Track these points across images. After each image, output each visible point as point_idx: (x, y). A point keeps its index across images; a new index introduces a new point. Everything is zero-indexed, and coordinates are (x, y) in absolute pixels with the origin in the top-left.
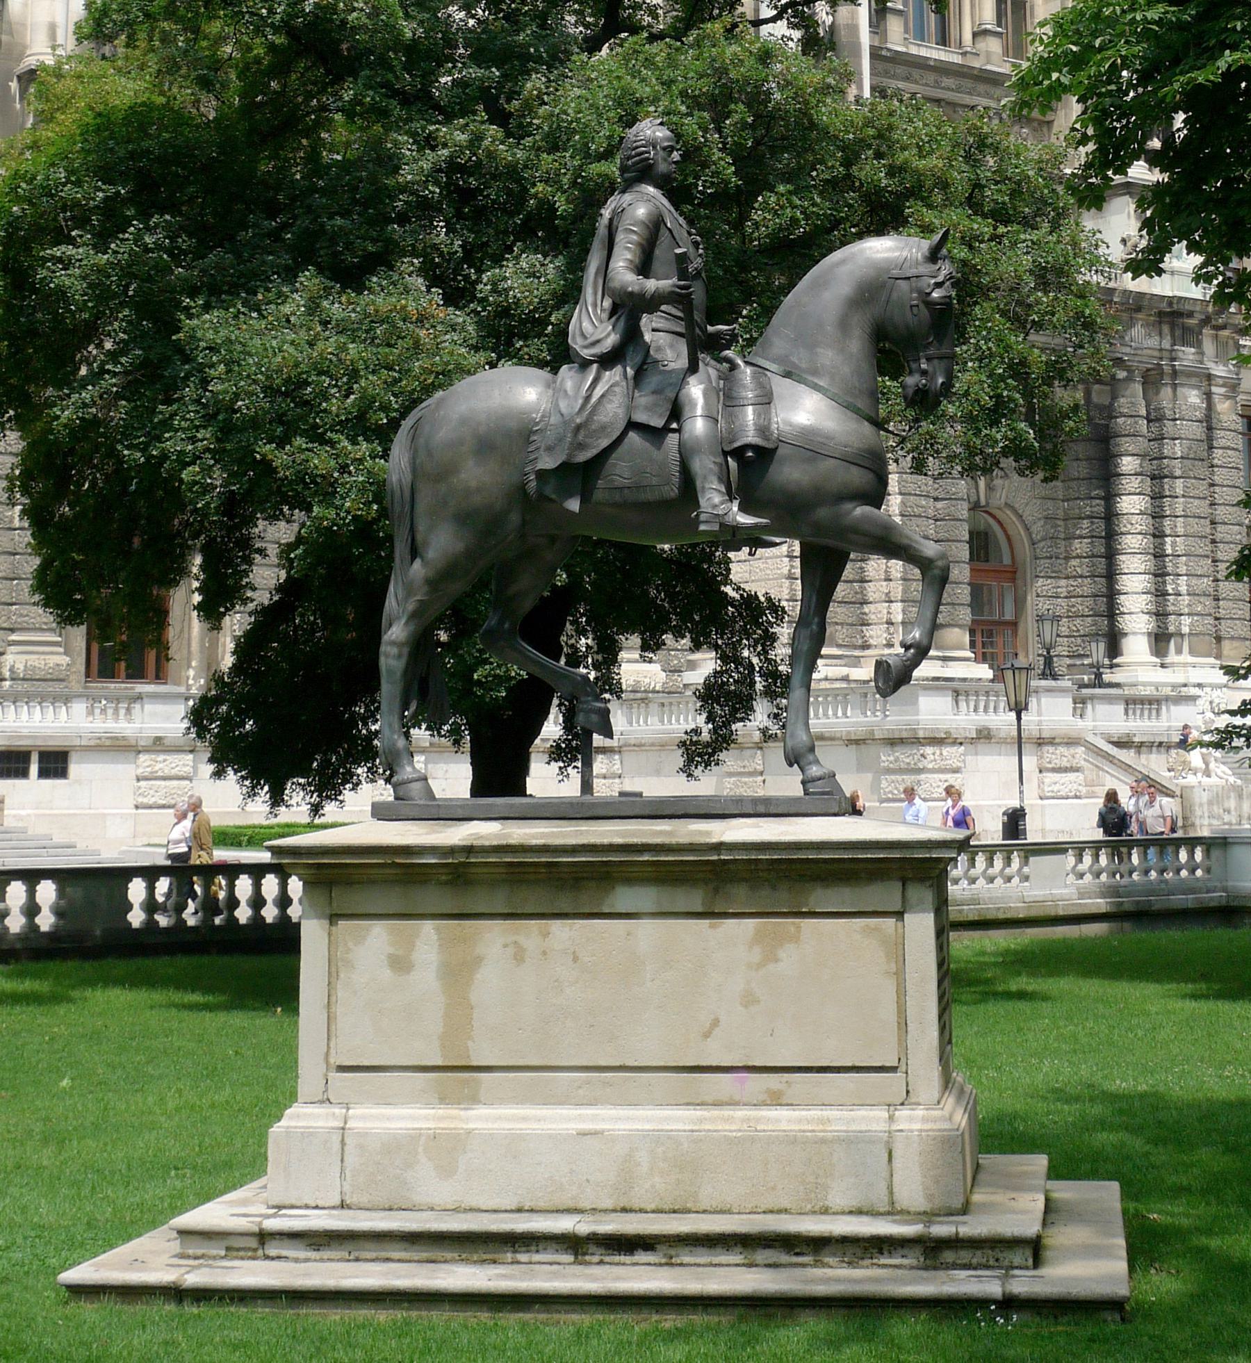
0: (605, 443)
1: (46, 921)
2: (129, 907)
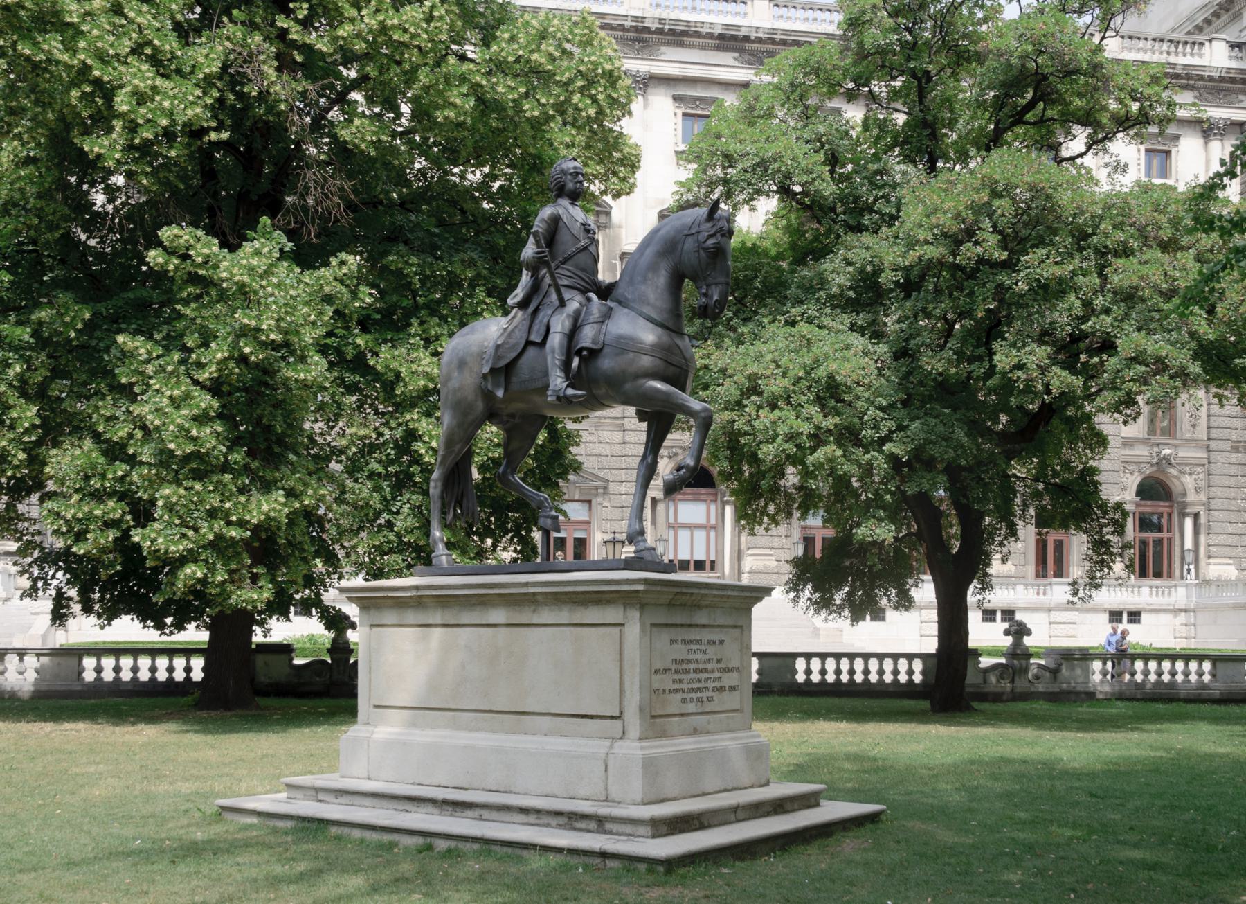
0: (514, 355)
1: (918, 678)
2: (797, 672)
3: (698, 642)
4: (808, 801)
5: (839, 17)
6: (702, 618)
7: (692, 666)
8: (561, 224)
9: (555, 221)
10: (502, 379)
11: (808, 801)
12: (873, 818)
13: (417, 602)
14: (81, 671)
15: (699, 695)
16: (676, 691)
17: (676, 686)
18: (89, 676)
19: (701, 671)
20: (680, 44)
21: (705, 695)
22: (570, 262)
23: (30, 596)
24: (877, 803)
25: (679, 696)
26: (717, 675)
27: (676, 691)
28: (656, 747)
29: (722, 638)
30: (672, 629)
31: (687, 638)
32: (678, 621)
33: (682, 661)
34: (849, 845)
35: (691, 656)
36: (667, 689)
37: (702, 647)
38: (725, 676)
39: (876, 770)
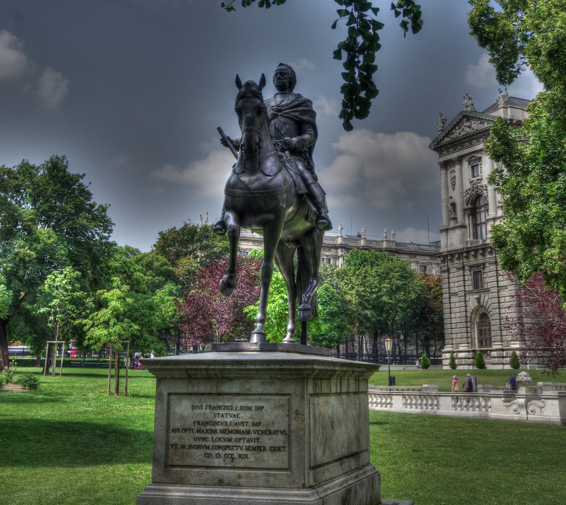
3: (231, 408)
5: (514, 291)
6: (226, 388)
7: (219, 428)
15: (228, 452)
16: (199, 447)
17: (198, 443)
19: (231, 432)
21: (236, 453)
26: (253, 436)
27: (199, 447)
28: (282, 495)
29: (260, 404)
30: (193, 398)
31: (213, 404)
32: (196, 390)
33: (207, 423)
36: (187, 444)
39: (260, 163)
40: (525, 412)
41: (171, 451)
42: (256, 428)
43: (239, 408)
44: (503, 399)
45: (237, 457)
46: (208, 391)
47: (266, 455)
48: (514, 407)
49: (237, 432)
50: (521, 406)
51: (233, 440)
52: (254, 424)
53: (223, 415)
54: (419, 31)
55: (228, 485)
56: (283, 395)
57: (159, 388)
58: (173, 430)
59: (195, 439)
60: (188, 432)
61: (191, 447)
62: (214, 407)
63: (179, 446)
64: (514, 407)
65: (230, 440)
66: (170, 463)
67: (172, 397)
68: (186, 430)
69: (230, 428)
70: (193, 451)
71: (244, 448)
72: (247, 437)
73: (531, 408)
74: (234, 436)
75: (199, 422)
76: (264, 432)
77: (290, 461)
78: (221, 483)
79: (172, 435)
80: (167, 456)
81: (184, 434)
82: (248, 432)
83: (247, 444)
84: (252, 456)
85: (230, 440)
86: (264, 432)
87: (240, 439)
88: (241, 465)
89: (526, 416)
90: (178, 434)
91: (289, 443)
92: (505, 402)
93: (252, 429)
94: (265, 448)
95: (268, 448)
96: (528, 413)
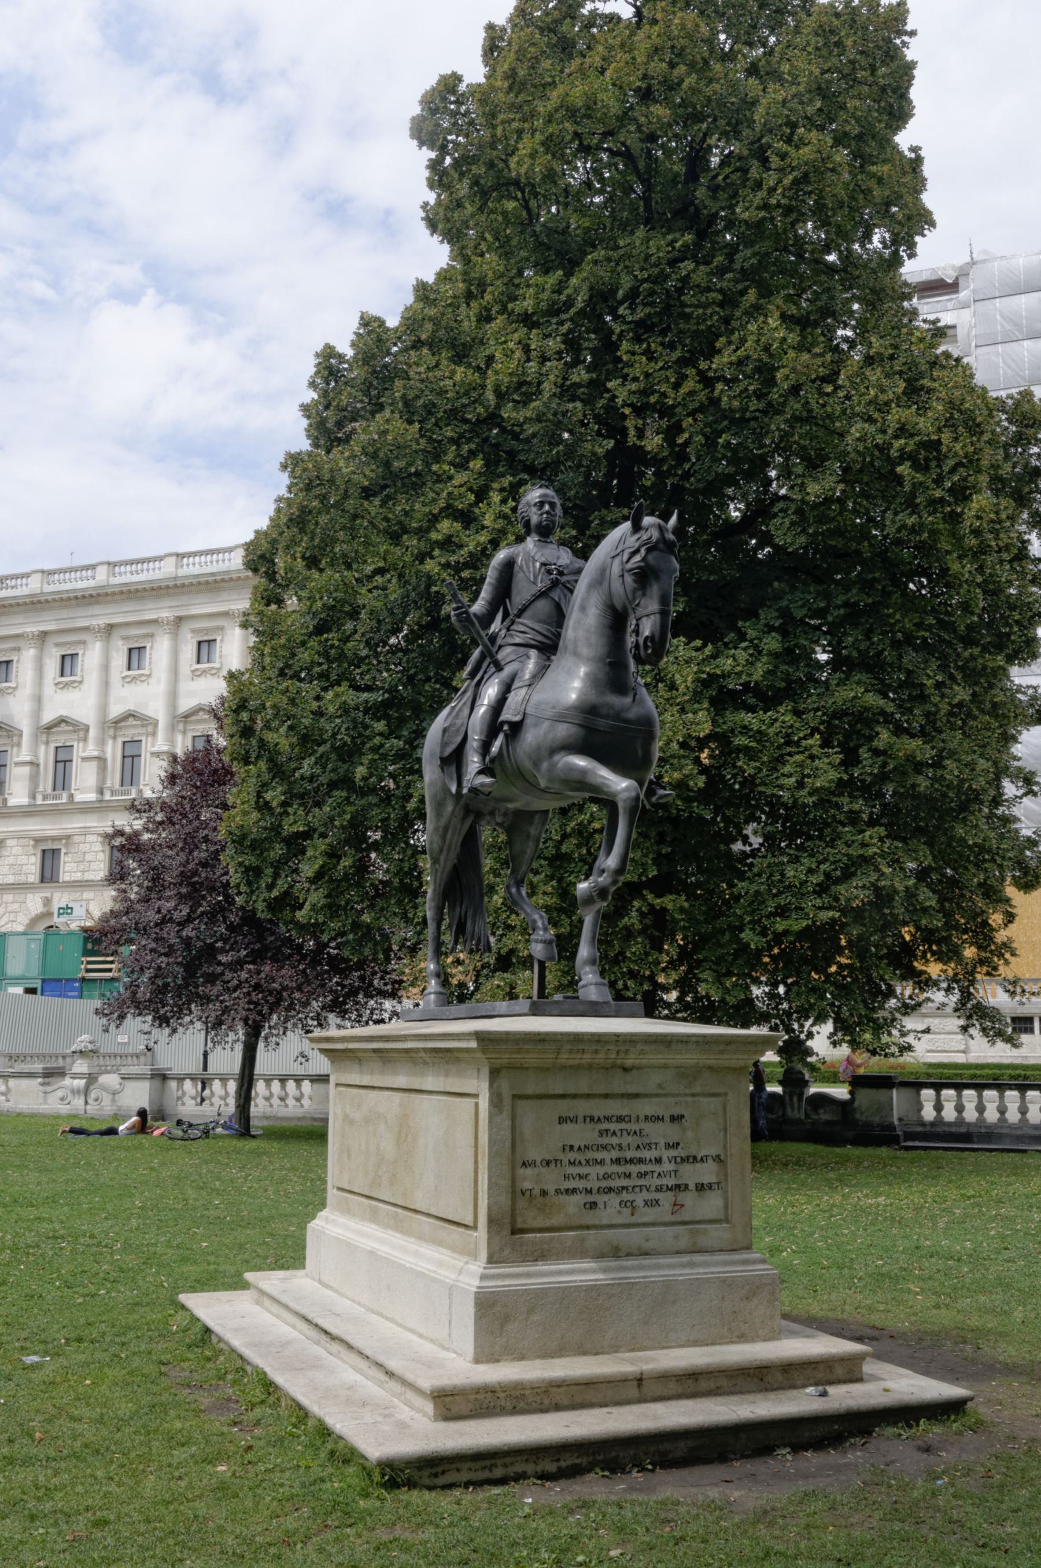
0: (459, 739)
4: (847, 1370)
8: (516, 568)
9: (509, 566)
10: (453, 769)
11: (847, 1370)
12: (952, 1408)
13: (385, 1056)
14: (920, 1107)
15: (626, 1197)
18: (928, 1113)
20: (98, 603)
21: (640, 1198)
22: (528, 613)
23: (1010, 922)
24: (955, 1380)
25: (579, 1199)
26: (667, 1167)
34: (894, 1446)
35: (605, 1140)
37: (633, 1127)
38: (687, 1169)
40: (82, 1101)
41: (522, 1203)
42: (673, 1153)
43: (642, 1117)
44: (40, 1080)
45: (642, 1204)
46: (586, 1090)
47: (688, 1199)
48: (60, 1093)
49: (641, 1161)
50: (75, 1092)
51: (634, 1175)
52: (668, 1146)
53: (614, 1133)
54: (930, 213)
55: (628, 1255)
56: (714, 1095)
57: (495, 1085)
58: (524, 1164)
59: (566, 1177)
60: (552, 1165)
61: (558, 1192)
62: (599, 1119)
63: (537, 1192)
64: (60, 1093)
65: (628, 1176)
66: (519, 1225)
67: (521, 1103)
68: (548, 1163)
69: (629, 1155)
70: (563, 1198)
71: (653, 1188)
72: (657, 1168)
73: (93, 1095)
74: (634, 1169)
75: (571, 1147)
76: (685, 1160)
77: (726, 1207)
78: (615, 1252)
79: (521, 1172)
80: (513, 1215)
81: (544, 1170)
82: (659, 1161)
83: (659, 1182)
84: (666, 1199)
85: (628, 1176)
86: (685, 1160)
87: (646, 1174)
88: (645, 1219)
89: (82, 1107)
90: (529, 1172)
91: (726, 1175)
92: (42, 1084)
93: (666, 1154)
94: (686, 1186)
95: (692, 1186)
96: (86, 1103)
